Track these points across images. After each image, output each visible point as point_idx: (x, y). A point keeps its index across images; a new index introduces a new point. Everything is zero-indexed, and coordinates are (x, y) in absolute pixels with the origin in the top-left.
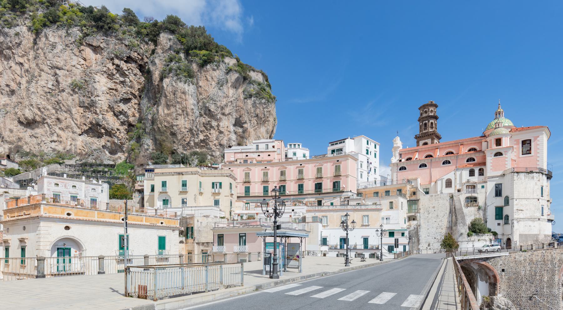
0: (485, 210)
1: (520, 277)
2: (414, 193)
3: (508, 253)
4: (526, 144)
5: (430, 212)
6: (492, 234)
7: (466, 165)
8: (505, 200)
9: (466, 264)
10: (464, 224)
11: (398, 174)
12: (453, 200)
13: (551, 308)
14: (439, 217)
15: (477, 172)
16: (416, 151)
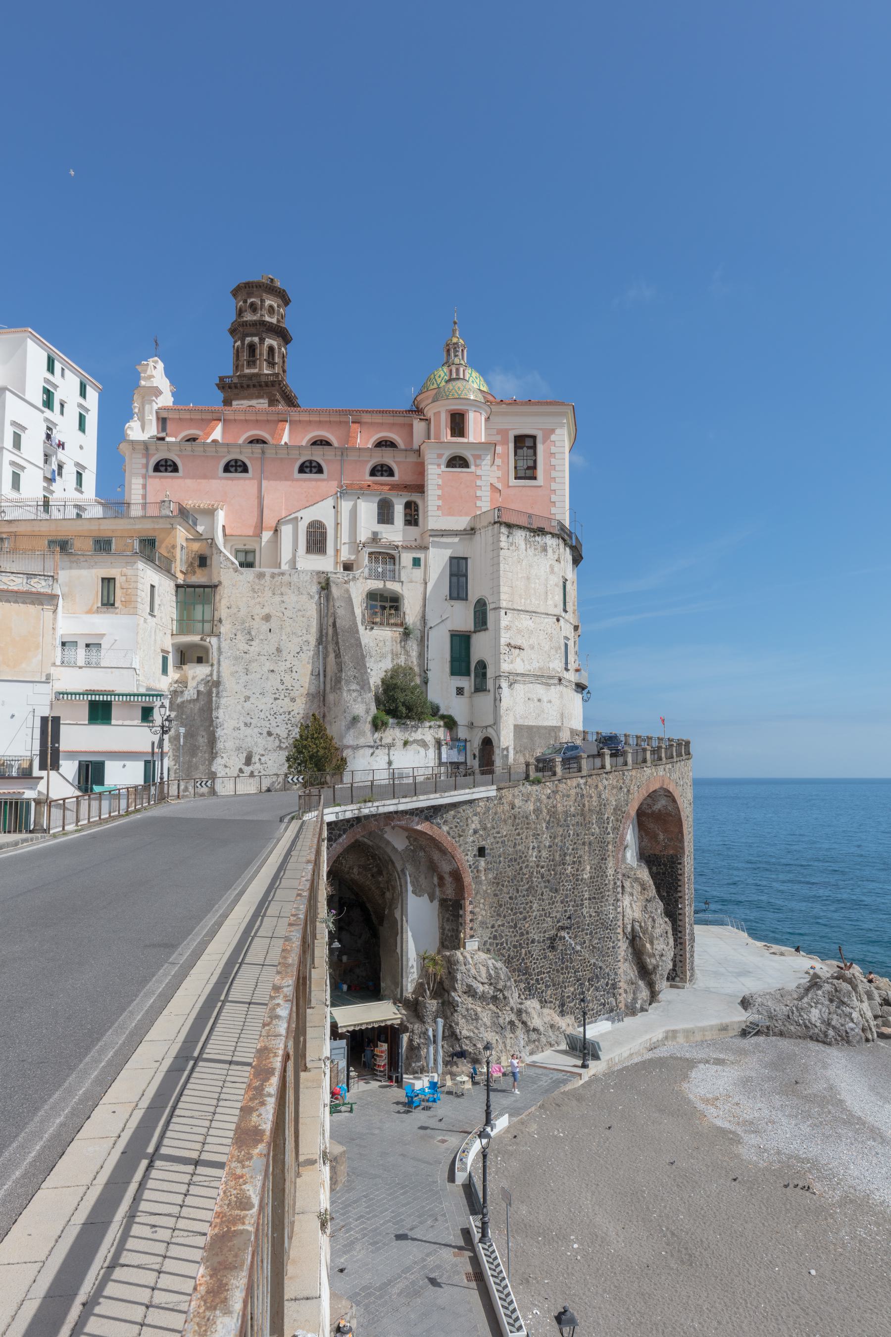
0: (422, 641)
1: (525, 871)
2: (203, 561)
3: (495, 787)
4: (525, 449)
5: (253, 633)
6: (442, 723)
7: (369, 483)
8: (475, 612)
9: (371, 834)
10: (364, 685)
11: (150, 482)
12: (328, 597)
13: (601, 968)
14: (284, 653)
15: (399, 510)
16: (215, 416)
